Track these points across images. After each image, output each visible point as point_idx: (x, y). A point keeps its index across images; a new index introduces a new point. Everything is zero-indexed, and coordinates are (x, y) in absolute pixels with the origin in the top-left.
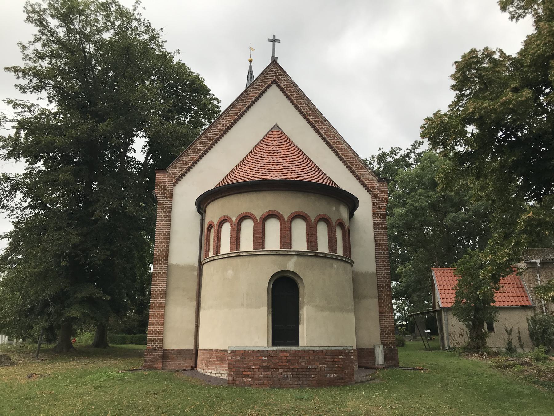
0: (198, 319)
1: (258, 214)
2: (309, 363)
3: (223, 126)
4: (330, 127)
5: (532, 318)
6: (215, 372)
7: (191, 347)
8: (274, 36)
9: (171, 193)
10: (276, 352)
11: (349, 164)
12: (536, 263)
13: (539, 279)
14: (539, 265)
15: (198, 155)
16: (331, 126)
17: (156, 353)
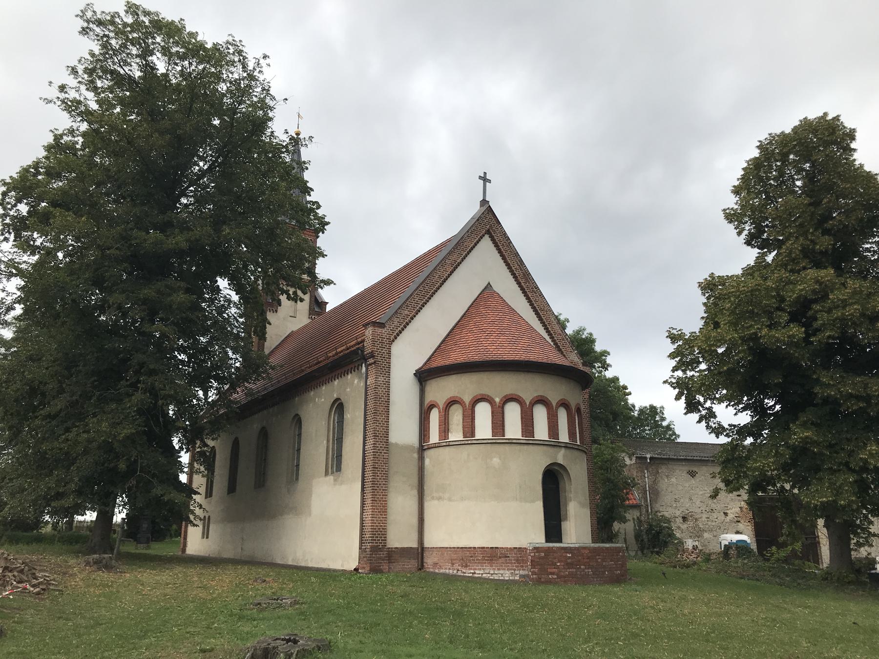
0: (421, 510)
1: (528, 398)
2: (603, 560)
3: (440, 277)
4: (540, 296)
5: (638, 518)
6: (482, 572)
7: (414, 545)
8: (485, 173)
9: (389, 353)
10: (595, 548)
11: (557, 341)
12: (646, 458)
13: (646, 475)
14: (649, 461)
15: (416, 309)
16: (541, 295)
17: (382, 551)
